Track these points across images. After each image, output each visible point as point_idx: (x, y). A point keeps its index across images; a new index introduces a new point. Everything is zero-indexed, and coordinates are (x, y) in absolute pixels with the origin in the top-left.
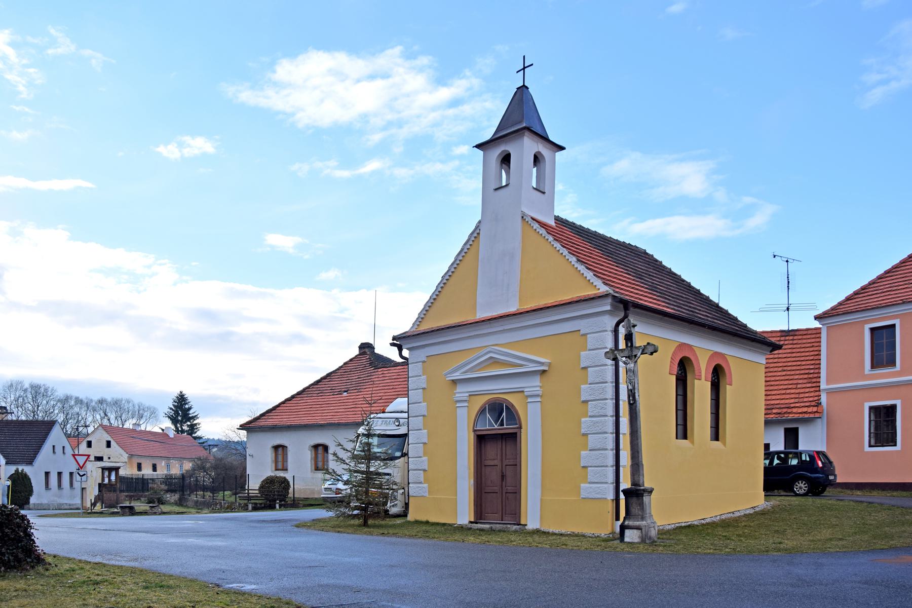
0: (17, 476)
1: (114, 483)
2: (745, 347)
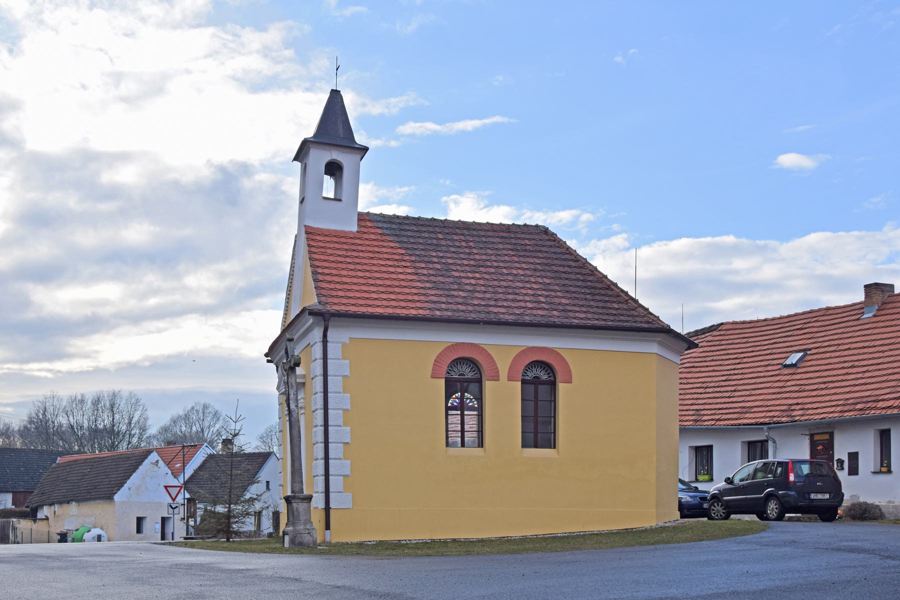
0: (71, 513)
1: (190, 519)
2: (653, 339)
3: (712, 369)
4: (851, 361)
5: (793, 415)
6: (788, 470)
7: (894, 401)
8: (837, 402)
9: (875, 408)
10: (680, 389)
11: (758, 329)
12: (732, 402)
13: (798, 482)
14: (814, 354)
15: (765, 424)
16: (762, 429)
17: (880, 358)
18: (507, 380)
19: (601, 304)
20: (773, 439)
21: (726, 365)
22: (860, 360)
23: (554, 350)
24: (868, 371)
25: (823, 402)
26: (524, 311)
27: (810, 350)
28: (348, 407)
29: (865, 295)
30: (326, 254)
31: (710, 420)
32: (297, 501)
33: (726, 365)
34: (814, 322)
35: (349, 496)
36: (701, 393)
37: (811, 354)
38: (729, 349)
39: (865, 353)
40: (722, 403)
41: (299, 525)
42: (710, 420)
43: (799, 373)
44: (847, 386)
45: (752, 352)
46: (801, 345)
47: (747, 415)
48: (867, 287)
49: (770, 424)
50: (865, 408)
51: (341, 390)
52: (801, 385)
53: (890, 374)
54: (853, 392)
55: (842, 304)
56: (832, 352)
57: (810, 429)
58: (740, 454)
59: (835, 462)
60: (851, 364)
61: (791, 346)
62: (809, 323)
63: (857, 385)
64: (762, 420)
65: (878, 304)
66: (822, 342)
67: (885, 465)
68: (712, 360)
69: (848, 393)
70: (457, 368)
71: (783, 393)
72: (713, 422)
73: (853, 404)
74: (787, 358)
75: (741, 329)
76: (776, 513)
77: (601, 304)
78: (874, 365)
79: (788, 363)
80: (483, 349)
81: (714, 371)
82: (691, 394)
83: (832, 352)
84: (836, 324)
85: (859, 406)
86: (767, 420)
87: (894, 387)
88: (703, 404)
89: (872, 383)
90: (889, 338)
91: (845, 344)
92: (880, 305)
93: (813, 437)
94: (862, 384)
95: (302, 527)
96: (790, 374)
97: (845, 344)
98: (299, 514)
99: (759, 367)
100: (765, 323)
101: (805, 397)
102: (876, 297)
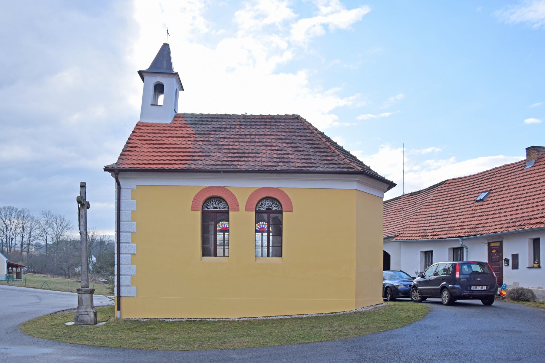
3: (437, 205)
4: (516, 195)
5: (477, 231)
6: (456, 269)
7: (541, 219)
8: (505, 221)
9: (529, 224)
10: (83, 186)
11: (465, 181)
12: (444, 224)
13: (462, 278)
14: (494, 193)
15: (461, 237)
16: (458, 240)
17: (535, 191)
18: (245, 210)
19: (319, 158)
20: (466, 246)
21: (445, 203)
22: (522, 194)
23: (280, 189)
24: (526, 201)
25: (496, 222)
26: (258, 163)
27: (492, 190)
28: (135, 230)
29: (526, 154)
30: (142, 136)
31: (431, 235)
32: (81, 293)
33: (445, 203)
34: (497, 174)
35: (134, 288)
36: (429, 220)
37: (492, 193)
38: (448, 194)
39: (525, 190)
40: (439, 225)
41: (82, 309)
42: (431, 235)
43: (484, 205)
44: (512, 211)
45: (460, 194)
46: (487, 188)
47: (451, 232)
48: (530, 150)
49: (463, 237)
50: (522, 225)
51: (130, 220)
52: (485, 212)
53: (540, 201)
54: (515, 214)
55: (514, 162)
56: (505, 190)
57: (488, 240)
58: (420, 257)
59: (504, 261)
60: (516, 197)
61: (482, 189)
62: (493, 175)
63: (518, 210)
64: (458, 235)
65: (535, 159)
66: (500, 185)
67: (536, 263)
68: (439, 201)
69: (512, 215)
70: (213, 204)
71: (473, 217)
72: (432, 237)
73: (514, 222)
74: (478, 196)
75: (456, 182)
76: (447, 300)
77: (319, 158)
78: (530, 196)
79: (478, 199)
80: (228, 190)
81: (438, 207)
82: (424, 220)
83: (505, 190)
84: (509, 174)
85: (518, 223)
86: (461, 234)
87: (542, 209)
88: (429, 226)
89: (528, 208)
90: (541, 179)
91: (513, 185)
92: (536, 159)
93: (490, 245)
94: (522, 209)
95: (84, 310)
96: (479, 206)
97: (513, 185)
98: (83, 301)
99: (462, 202)
100: (470, 178)
101: (486, 219)
102: (534, 155)
